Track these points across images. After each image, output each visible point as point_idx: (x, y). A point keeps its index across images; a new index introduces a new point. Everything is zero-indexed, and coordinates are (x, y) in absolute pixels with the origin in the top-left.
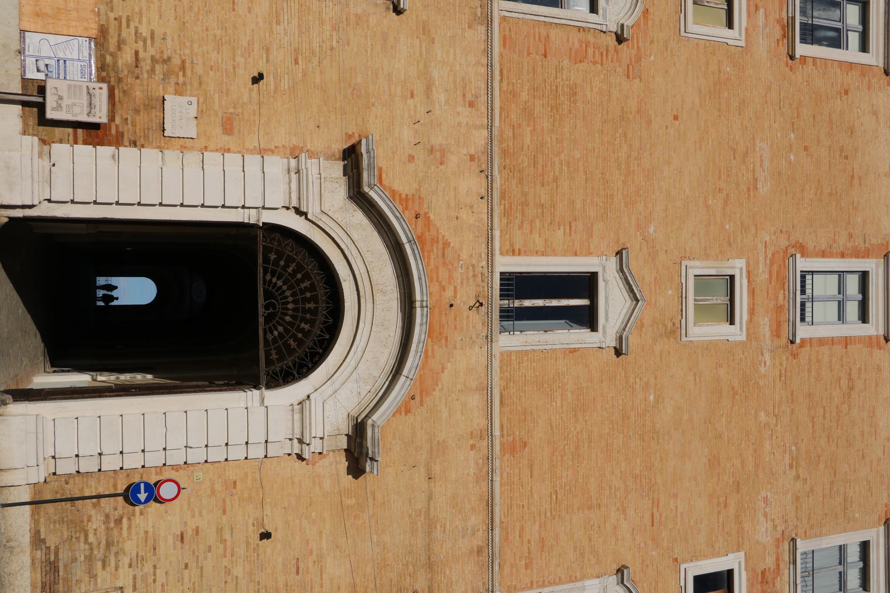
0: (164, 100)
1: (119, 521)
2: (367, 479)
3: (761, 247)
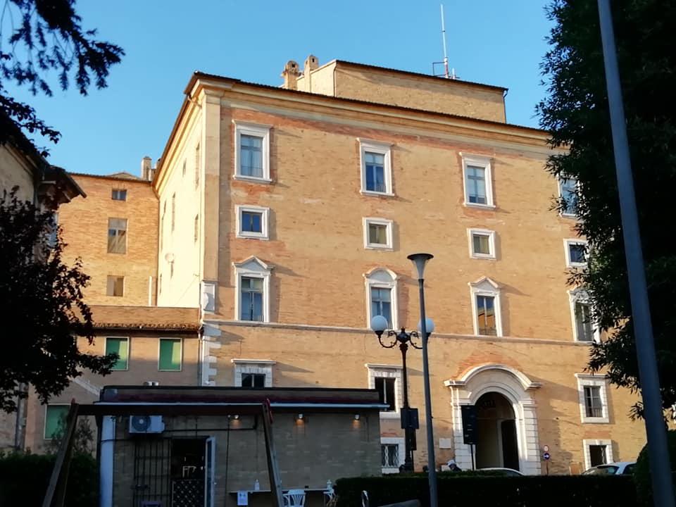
0: (442, 449)
1: (553, 463)
2: (20, 87)
3: (463, 220)
